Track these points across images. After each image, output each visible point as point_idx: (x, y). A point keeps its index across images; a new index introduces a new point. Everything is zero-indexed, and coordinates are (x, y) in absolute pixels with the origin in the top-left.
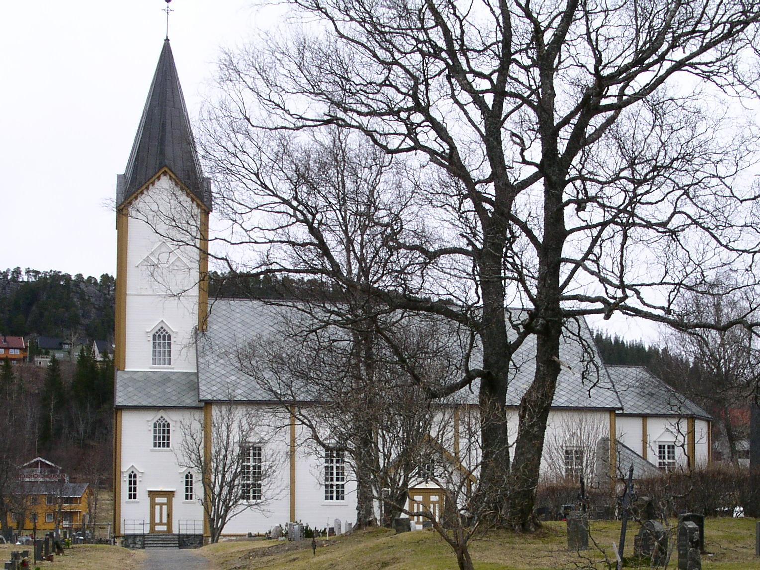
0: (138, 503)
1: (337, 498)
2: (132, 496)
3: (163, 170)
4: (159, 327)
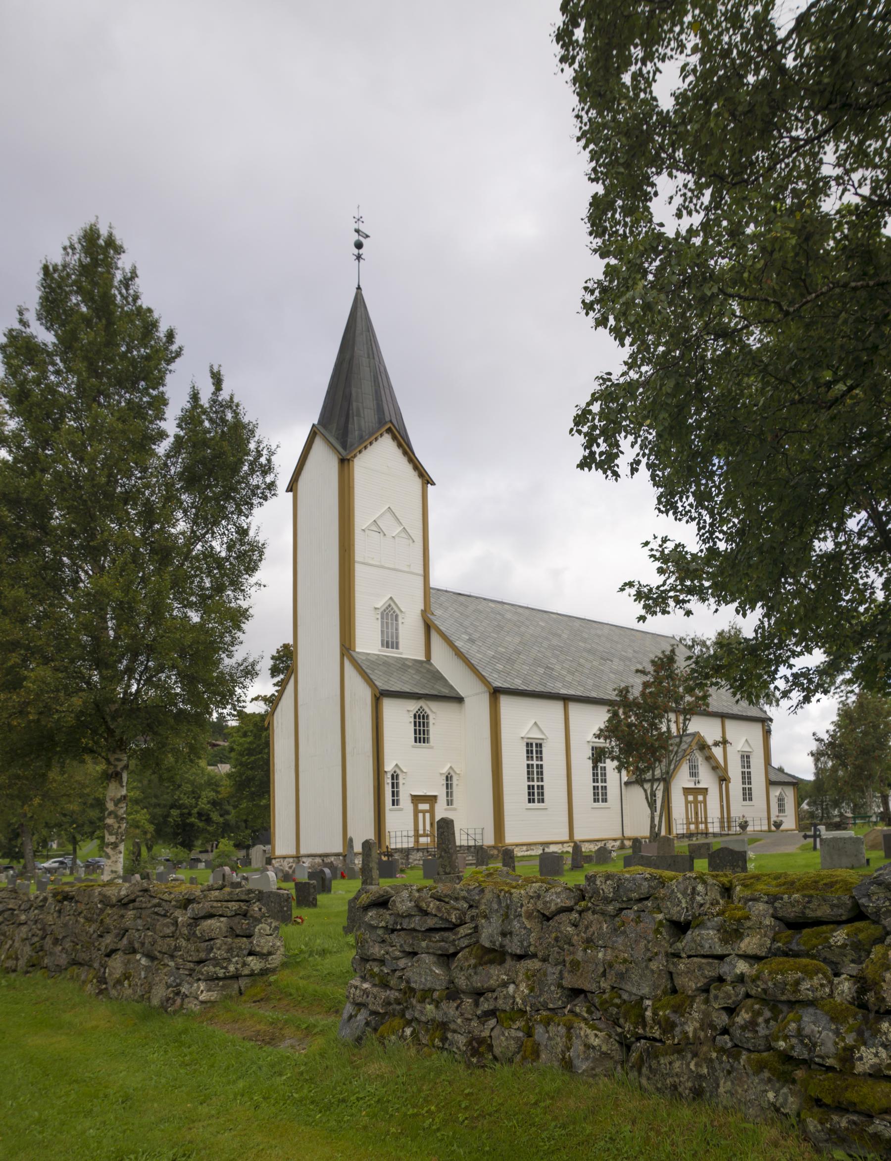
0: (401, 810)
1: (539, 802)
2: (395, 802)
3: (387, 427)
4: (387, 605)
